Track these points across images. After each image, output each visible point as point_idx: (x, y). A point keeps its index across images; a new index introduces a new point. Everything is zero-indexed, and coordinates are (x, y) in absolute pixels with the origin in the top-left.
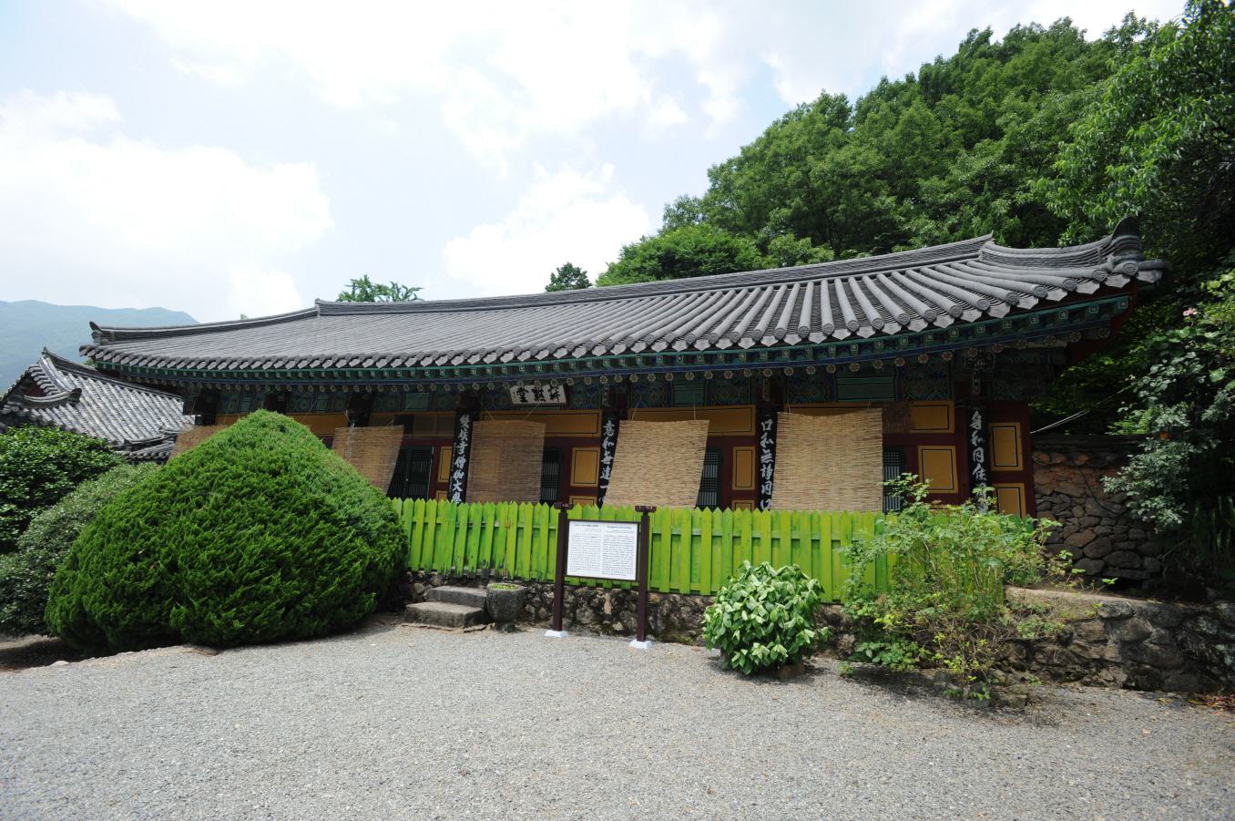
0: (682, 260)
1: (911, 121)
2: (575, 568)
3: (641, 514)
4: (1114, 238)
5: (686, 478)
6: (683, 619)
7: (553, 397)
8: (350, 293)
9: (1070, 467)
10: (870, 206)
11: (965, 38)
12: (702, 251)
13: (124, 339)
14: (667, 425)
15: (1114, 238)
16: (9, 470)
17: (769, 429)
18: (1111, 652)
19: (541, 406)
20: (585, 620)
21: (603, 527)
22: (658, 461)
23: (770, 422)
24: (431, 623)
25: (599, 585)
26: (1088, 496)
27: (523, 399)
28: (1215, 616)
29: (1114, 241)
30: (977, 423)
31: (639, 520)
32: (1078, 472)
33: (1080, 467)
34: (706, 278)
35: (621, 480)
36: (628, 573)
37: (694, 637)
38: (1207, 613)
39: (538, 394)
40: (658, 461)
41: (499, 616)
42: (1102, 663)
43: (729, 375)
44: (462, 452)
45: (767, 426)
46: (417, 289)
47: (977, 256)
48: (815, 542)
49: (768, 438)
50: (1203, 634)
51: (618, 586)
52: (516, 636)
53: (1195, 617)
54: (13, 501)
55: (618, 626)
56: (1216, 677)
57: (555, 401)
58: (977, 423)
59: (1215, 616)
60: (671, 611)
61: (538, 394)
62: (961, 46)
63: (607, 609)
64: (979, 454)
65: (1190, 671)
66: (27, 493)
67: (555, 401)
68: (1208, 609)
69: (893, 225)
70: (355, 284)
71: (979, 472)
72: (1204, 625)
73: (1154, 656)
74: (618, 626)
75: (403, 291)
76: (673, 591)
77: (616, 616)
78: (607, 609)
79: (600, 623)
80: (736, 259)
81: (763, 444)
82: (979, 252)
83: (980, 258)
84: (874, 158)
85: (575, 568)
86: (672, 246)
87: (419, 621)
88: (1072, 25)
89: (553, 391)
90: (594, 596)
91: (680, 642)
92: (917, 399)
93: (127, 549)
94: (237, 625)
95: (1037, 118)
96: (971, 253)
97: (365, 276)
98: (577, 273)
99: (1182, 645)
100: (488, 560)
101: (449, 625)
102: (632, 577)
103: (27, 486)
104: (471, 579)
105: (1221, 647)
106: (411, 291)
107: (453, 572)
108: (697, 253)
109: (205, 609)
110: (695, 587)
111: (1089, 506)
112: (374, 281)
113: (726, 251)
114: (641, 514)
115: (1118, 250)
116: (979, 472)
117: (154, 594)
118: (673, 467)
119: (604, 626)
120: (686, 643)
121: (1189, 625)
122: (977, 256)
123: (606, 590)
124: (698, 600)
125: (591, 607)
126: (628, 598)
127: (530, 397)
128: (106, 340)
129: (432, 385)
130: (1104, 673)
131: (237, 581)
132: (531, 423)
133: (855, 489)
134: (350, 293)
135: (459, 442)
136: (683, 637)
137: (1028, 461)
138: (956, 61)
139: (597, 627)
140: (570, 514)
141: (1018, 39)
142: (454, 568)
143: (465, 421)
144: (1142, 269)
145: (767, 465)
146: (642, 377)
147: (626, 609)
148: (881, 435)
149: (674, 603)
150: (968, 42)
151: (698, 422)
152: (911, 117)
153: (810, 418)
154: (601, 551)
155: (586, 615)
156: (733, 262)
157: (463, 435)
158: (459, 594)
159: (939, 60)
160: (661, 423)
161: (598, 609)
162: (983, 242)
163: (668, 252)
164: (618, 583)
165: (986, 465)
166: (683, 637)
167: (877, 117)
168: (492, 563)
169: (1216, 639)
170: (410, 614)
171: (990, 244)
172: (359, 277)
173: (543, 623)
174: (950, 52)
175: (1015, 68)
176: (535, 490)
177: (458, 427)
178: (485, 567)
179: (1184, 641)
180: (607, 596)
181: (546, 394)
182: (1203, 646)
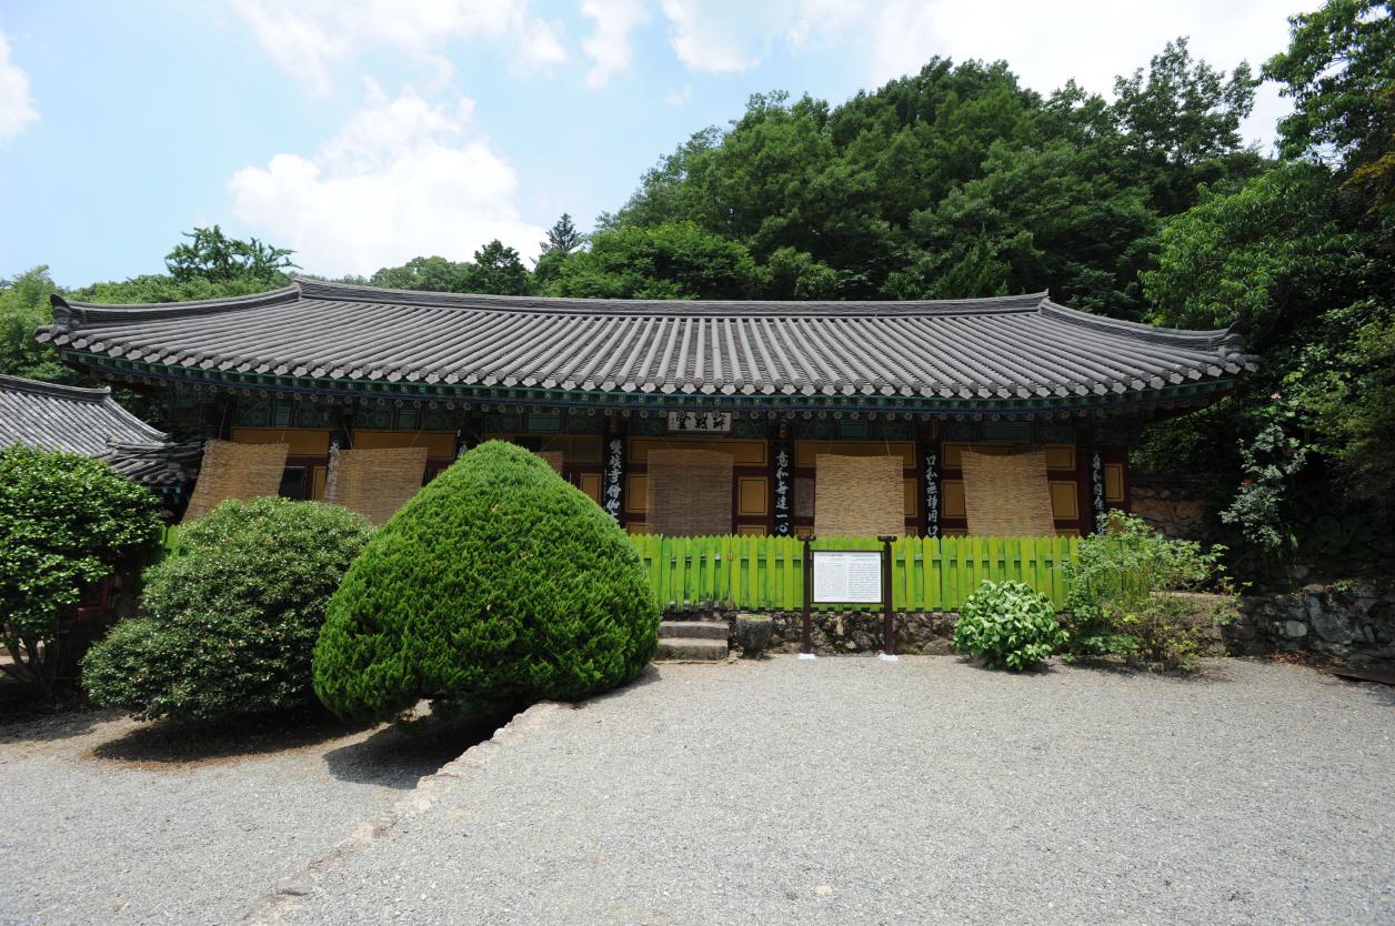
0: (679, 262)
1: (901, 148)
2: (821, 595)
3: (883, 543)
4: (1228, 334)
5: (890, 509)
6: (911, 633)
7: (716, 425)
8: (191, 246)
9: (1156, 499)
10: (867, 227)
11: (928, 63)
12: (701, 254)
13: (116, 321)
14: (863, 459)
15: (1228, 334)
16: (39, 507)
17: (933, 463)
18: (1216, 633)
19: (703, 433)
20: (818, 642)
21: (848, 558)
22: (860, 492)
23: (934, 457)
24: (687, 658)
25: (831, 609)
26: (1167, 521)
27: (682, 425)
28: (1274, 603)
29: (1228, 338)
30: (1097, 465)
31: (882, 549)
32: (1162, 503)
33: (1162, 499)
34: (797, 303)
35: (826, 511)
36: (875, 596)
37: (920, 648)
38: (1268, 602)
39: (701, 422)
40: (860, 492)
41: (753, 644)
42: (1213, 641)
43: (891, 417)
44: (615, 480)
45: (931, 460)
46: (289, 252)
47: (1036, 311)
48: (1017, 563)
49: (933, 471)
50: (1267, 615)
51: (849, 609)
52: (762, 664)
53: (1262, 605)
54: (56, 550)
55: (851, 645)
56: (1273, 643)
57: (718, 429)
58: (1097, 465)
59: (1274, 603)
60: (899, 627)
61: (701, 422)
62: (923, 68)
63: (840, 630)
64: (1098, 489)
65: (1259, 641)
66: (71, 538)
67: (718, 429)
68: (1269, 599)
69: (885, 249)
70: (201, 235)
71: (1099, 503)
72: (1268, 610)
73: (1241, 633)
74: (851, 645)
75: (268, 252)
76: (919, 610)
77: (848, 636)
78: (840, 630)
79: (833, 643)
80: (736, 267)
81: (928, 476)
82: (1039, 307)
83: (1039, 312)
84: (870, 178)
85: (821, 595)
86: (667, 244)
87: (674, 658)
88: (1008, 69)
89: (719, 420)
90: (826, 620)
91: (909, 653)
92: (1048, 441)
93: (470, 606)
94: (598, 675)
95: (1020, 168)
96: (1030, 307)
97: (216, 227)
98: (508, 254)
99: (1255, 624)
100: (711, 593)
101: (709, 658)
102: (878, 599)
103: (69, 528)
104: (693, 613)
105: (1277, 624)
106: (280, 253)
107: (672, 607)
108: (697, 256)
109: (570, 663)
110: (920, 605)
111: (1168, 529)
112: (229, 235)
113: (727, 256)
114: (883, 543)
115: (1229, 344)
116: (1099, 503)
117: (514, 652)
118: (875, 499)
119: (837, 645)
120: (914, 653)
121: (1259, 610)
122: (1036, 311)
123: (837, 613)
124: (922, 616)
125: (824, 630)
126: (859, 619)
127: (691, 425)
128: (76, 322)
129: (607, 409)
130: (1211, 648)
131: (588, 632)
132: (716, 454)
133: (1032, 518)
134: (191, 246)
135: (610, 469)
136: (912, 649)
137: (1127, 494)
138: (917, 83)
139: (831, 647)
140: (813, 545)
141: (968, 70)
142: (673, 603)
143: (616, 446)
144: (1248, 361)
145: (932, 496)
146: (815, 415)
147: (858, 629)
148: (1045, 473)
149: (901, 621)
150: (930, 67)
151: (893, 458)
152: (903, 143)
153: (989, 457)
154: (847, 578)
155: (820, 637)
156: (732, 270)
157: (615, 462)
158: (699, 628)
159: (904, 78)
160: (857, 458)
161: (830, 631)
162: (1041, 298)
163: (662, 250)
164: (849, 606)
165: (1103, 498)
166: (912, 649)
167: (870, 136)
168: (716, 596)
169: (1275, 618)
170: (661, 652)
171: (1047, 300)
172: (207, 225)
173: (777, 649)
174: (914, 72)
175: (982, 110)
176: (727, 520)
177: (608, 454)
178: (708, 600)
179: (1257, 621)
180: (838, 619)
181: (710, 422)
182: (1267, 624)
